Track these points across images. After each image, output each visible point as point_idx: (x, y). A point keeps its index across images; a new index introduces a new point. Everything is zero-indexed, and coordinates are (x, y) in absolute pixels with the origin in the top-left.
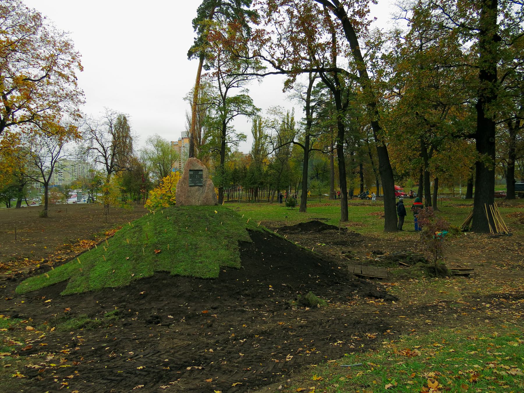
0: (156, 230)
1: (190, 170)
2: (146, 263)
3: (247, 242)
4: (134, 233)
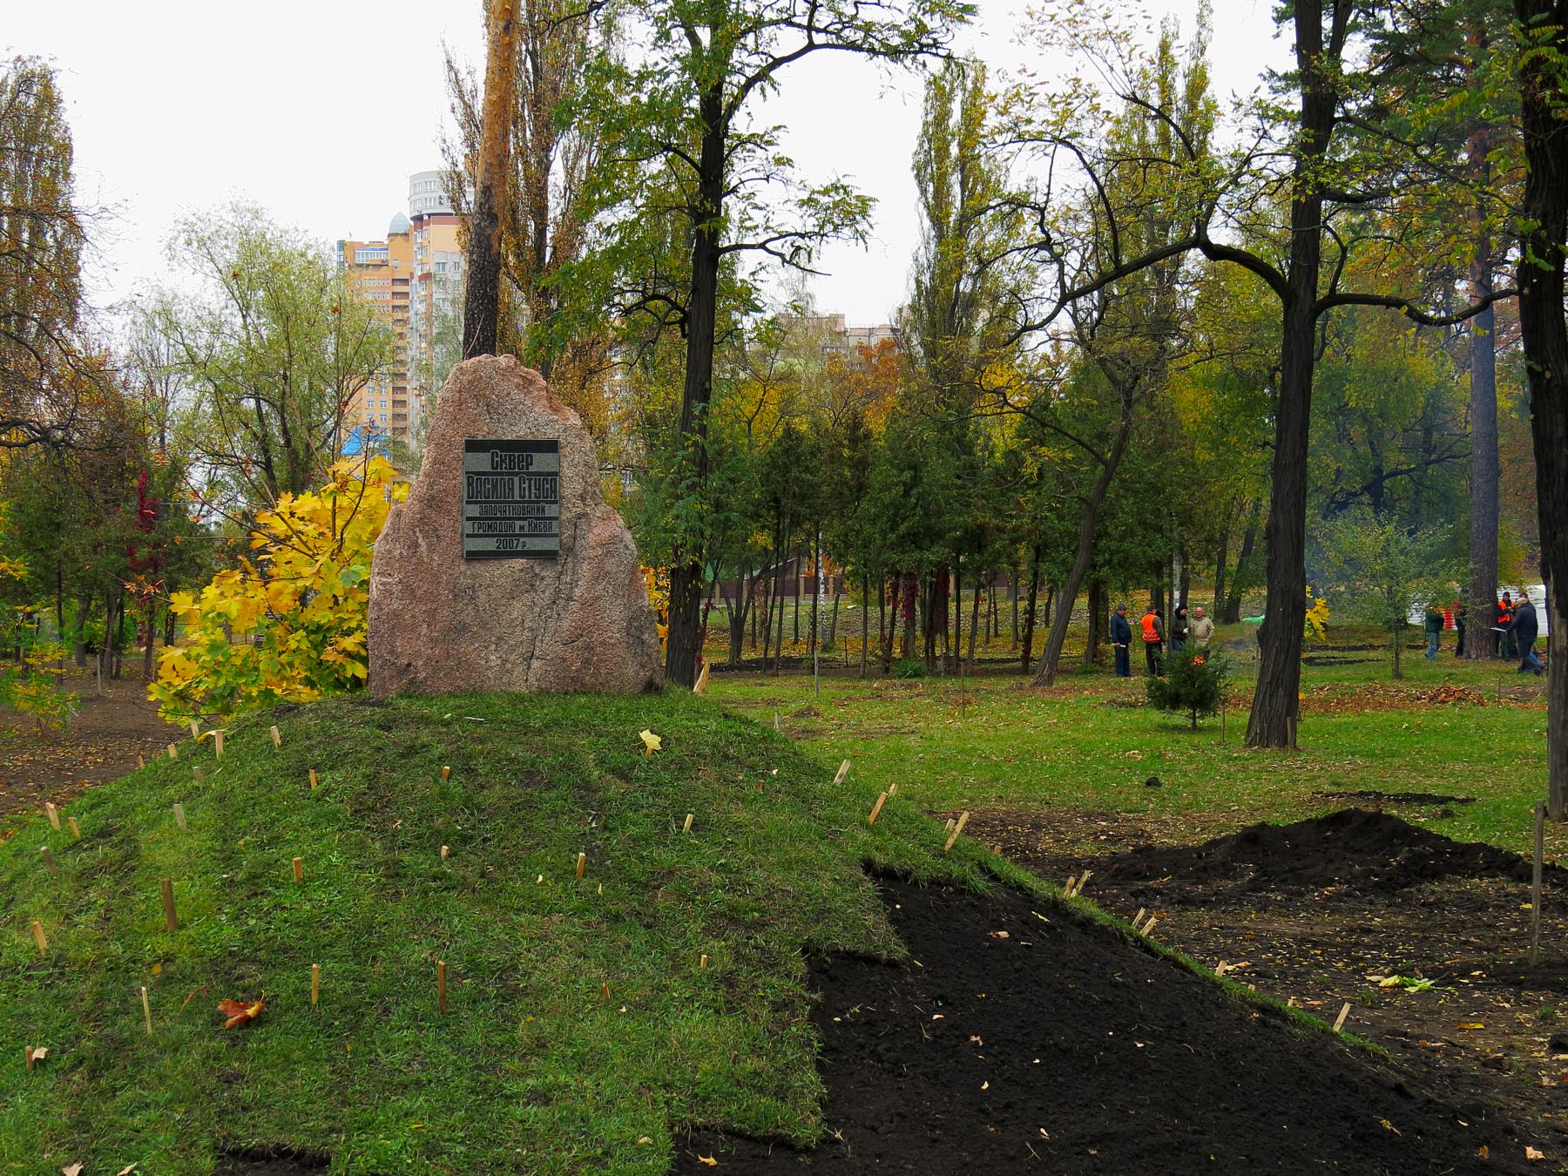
0: (229, 859)
1: (473, 446)
3: (871, 960)
4: (85, 877)
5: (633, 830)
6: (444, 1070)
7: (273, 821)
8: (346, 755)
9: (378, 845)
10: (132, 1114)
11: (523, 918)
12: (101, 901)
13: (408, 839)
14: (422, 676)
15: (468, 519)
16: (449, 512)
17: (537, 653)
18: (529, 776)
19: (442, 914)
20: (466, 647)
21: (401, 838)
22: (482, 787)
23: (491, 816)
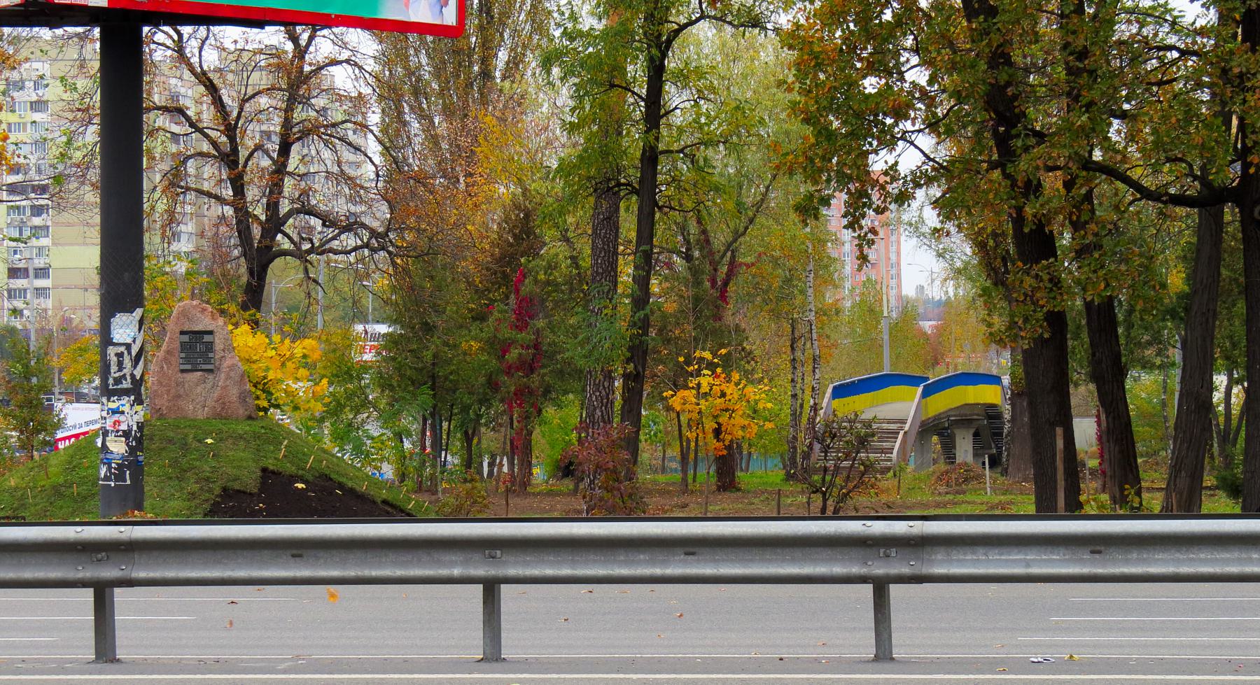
1: (182, 333)
3: (244, 492)
20: (181, 403)
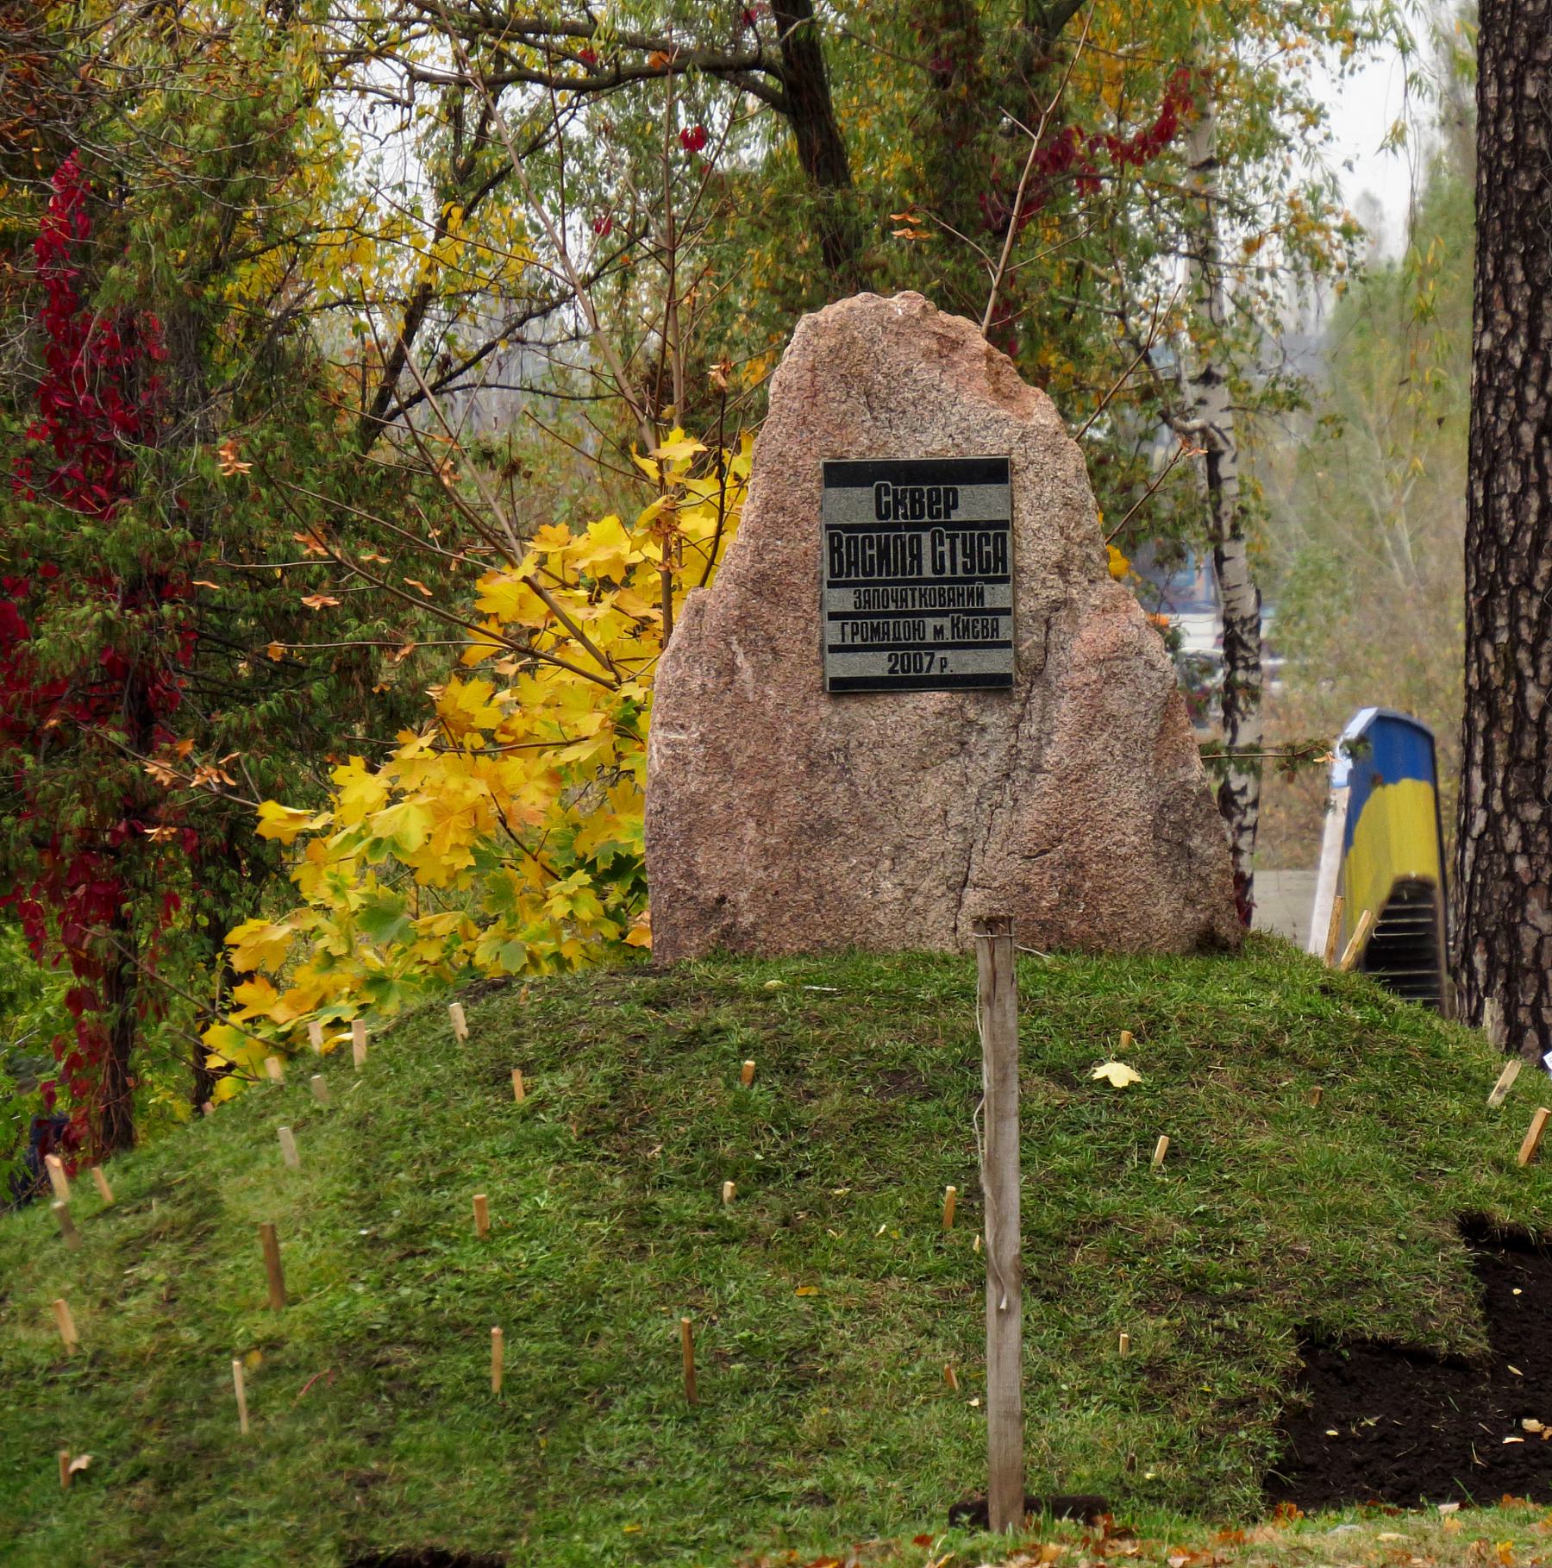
0: (372, 1208)
1: (839, 474)
2: (268, 1501)
3: (1420, 1357)
4: (134, 1248)
5: (1061, 1162)
6: (683, 1470)
7: (446, 1152)
8: (579, 1046)
9: (618, 1182)
10: (222, 1525)
11: (840, 1283)
12: (162, 1277)
13: (669, 1173)
14: (747, 920)
15: (833, 616)
16: (796, 604)
17: (974, 875)
18: (899, 1077)
19: (711, 1278)
20: (836, 867)
21: (658, 1172)
22: (810, 1095)
23: (817, 1139)
